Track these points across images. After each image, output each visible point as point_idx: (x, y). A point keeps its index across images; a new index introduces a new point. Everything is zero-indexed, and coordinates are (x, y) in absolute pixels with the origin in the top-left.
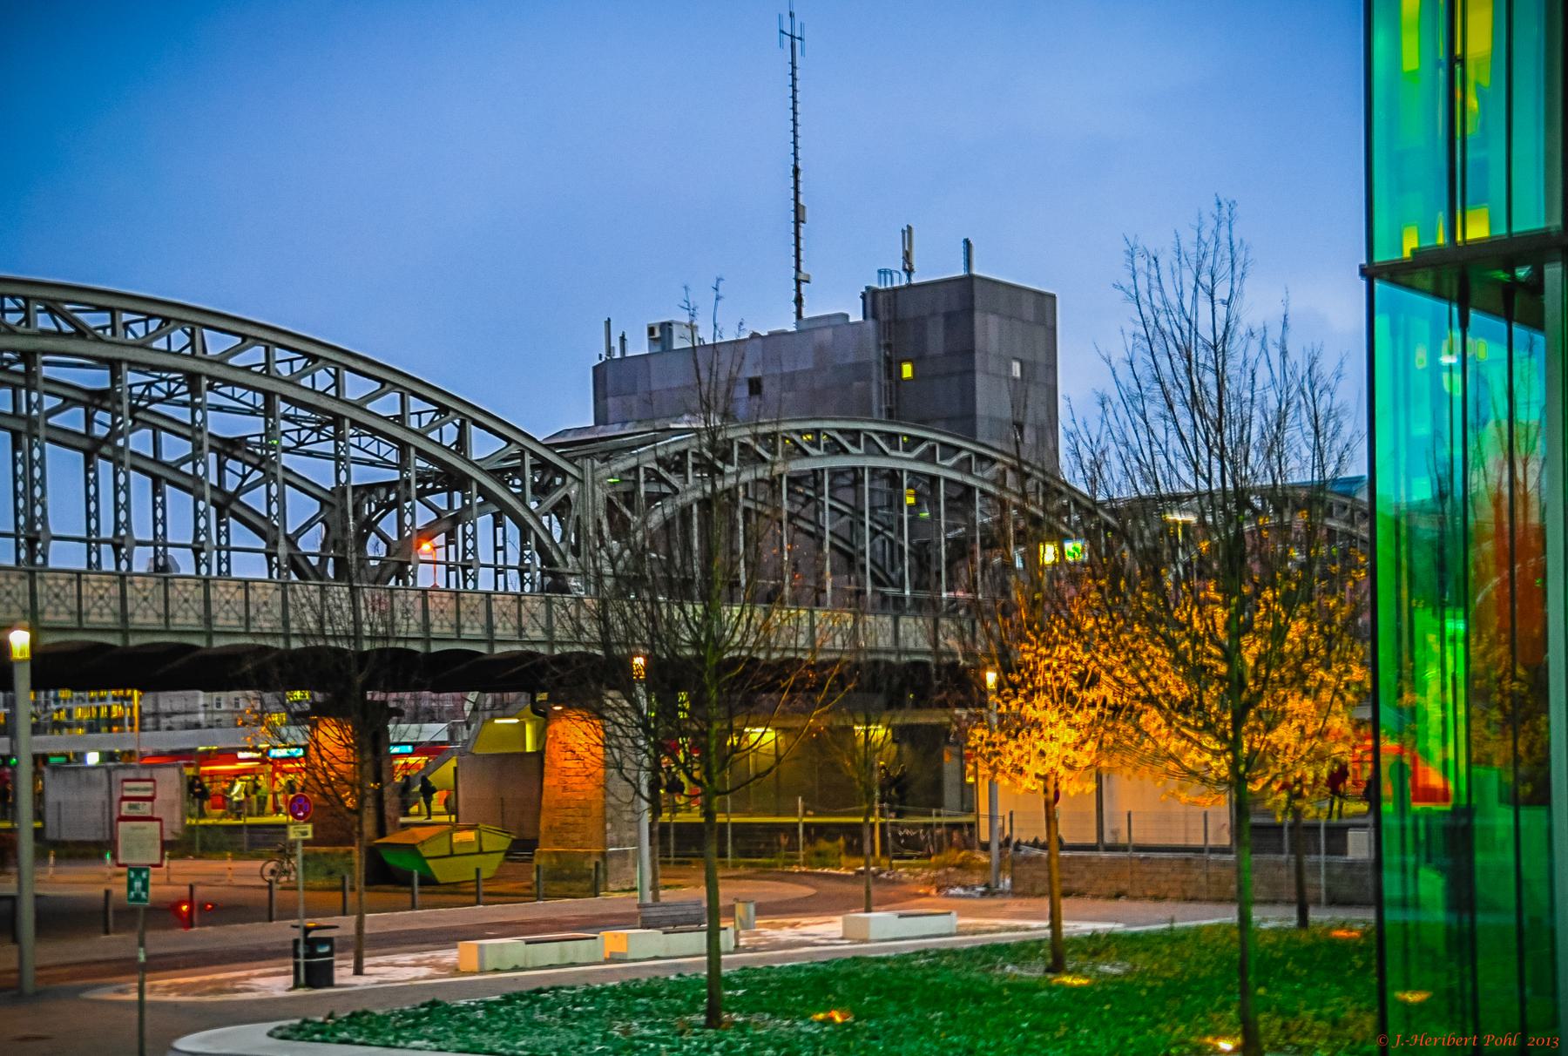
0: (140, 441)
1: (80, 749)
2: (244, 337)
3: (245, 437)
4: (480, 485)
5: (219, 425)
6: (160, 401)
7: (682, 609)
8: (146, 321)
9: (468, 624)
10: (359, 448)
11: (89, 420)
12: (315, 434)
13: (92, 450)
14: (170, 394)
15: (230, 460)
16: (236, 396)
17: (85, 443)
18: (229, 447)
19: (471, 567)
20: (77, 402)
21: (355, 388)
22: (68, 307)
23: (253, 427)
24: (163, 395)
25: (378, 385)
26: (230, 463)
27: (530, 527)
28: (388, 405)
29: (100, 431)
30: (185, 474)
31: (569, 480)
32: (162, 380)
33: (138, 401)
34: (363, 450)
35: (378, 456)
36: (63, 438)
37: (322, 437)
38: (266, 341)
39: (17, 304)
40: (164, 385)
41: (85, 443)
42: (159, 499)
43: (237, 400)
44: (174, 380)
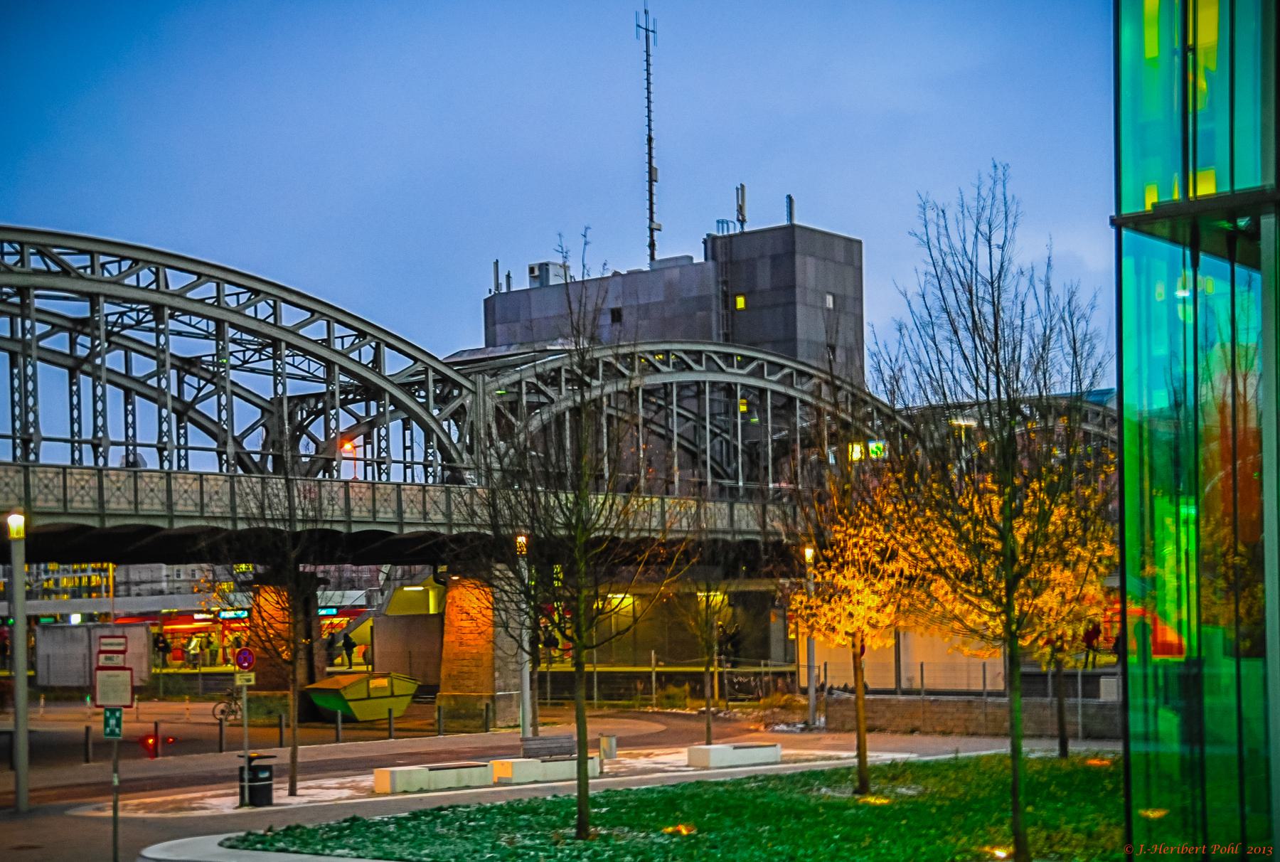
0: (114, 360)
1: (65, 611)
2: (200, 275)
3: (200, 357)
4: (392, 396)
5: (179, 347)
6: (131, 327)
7: (557, 497)
8: (119, 262)
9: (382, 509)
10: (293, 365)
11: (73, 343)
12: (257, 355)
13: (75, 367)
14: (139, 322)
15: (187, 376)
16: (193, 323)
17: (70, 362)
18: (187, 365)
19: (384, 463)
20: (63, 329)
21: (290, 316)
22: (55, 250)
23: (206, 349)
24: (133, 323)
25: (308, 314)
26: (188, 378)
27: (433, 431)
28: (316, 331)
29: (82, 352)
30: (151, 387)
31: (465, 392)
32: (132, 310)
33: (113, 327)
34: (296, 367)
35: (308, 372)
36: (51, 358)
37: (263, 357)
38: (217, 278)
39: (14, 248)
40: (134, 315)
41: (70, 362)
42: (130, 407)
43: (194, 327)
44: (142, 310)
